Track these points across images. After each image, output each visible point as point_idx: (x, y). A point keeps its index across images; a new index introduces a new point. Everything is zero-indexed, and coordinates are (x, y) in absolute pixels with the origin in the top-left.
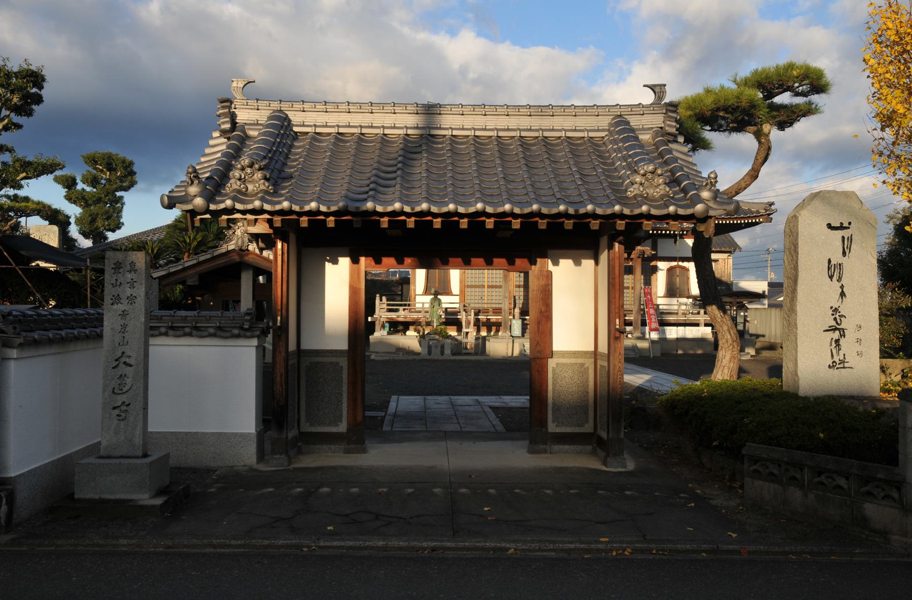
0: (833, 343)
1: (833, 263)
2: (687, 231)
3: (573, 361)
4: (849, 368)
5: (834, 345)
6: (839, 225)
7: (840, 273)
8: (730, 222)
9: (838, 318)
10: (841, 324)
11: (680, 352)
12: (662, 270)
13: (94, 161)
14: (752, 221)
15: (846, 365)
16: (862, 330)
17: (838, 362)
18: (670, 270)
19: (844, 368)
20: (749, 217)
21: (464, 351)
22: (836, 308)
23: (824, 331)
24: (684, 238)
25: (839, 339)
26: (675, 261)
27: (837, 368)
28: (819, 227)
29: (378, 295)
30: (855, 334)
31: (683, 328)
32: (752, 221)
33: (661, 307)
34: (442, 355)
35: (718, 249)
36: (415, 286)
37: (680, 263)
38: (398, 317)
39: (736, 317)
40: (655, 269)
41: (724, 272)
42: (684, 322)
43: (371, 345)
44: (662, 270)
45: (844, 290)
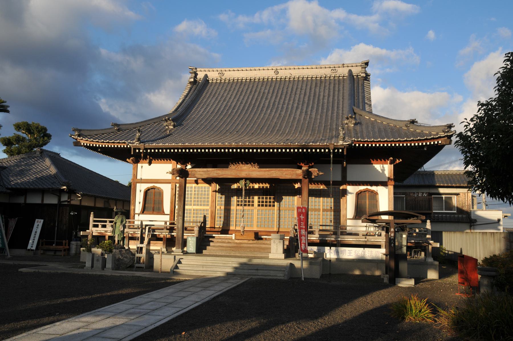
3: (223, 278)
11: (357, 272)
12: (351, 193)
13: (19, 127)
18: (359, 194)
21: (137, 265)
24: (372, 164)
26: (364, 185)
29: (92, 213)
31: (362, 249)
33: (348, 228)
35: (458, 185)
37: (369, 187)
38: (106, 231)
39: (394, 240)
40: (345, 193)
41: (465, 203)
42: (364, 243)
44: (351, 193)
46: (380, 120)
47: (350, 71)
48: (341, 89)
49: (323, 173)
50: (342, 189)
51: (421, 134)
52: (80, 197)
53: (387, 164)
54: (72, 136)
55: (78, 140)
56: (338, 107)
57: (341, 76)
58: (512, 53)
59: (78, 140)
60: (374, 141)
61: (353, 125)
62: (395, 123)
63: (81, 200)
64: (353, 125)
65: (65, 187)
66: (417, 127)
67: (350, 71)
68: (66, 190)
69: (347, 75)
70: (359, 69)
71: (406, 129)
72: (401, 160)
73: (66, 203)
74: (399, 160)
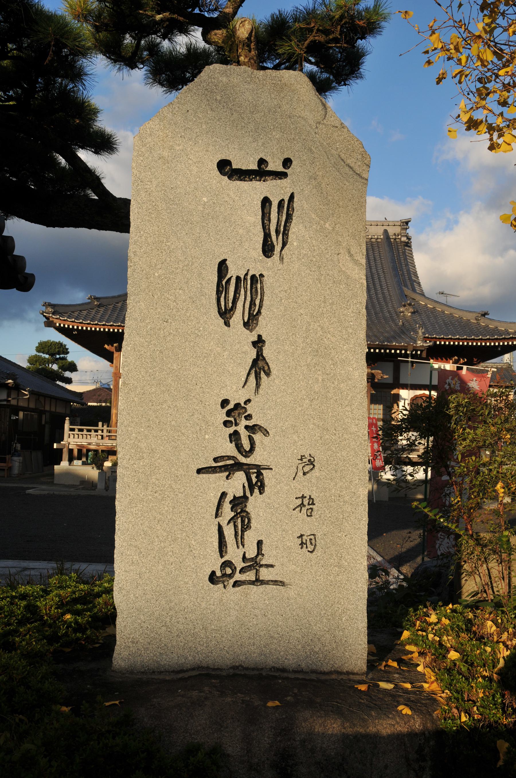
0: (227, 506)
1: (233, 272)
2: (422, 351)
4: (275, 582)
5: (227, 512)
6: (254, 167)
7: (252, 303)
8: (481, 343)
9: (244, 434)
10: (252, 449)
14: (508, 343)
15: (265, 574)
16: (316, 472)
17: (240, 565)
19: (258, 581)
20: (505, 339)
22: (237, 406)
23: (199, 471)
25: (245, 498)
26: (420, 389)
27: (236, 584)
28: (195, 169)
30: (295, 483)
32: (508, 343)
34: (107, 490)
36: (117, 409)
43: (55, 476)
45: (266, 352)
46: (440, 308)
47: (386, 231)
48: (378, 258)
49: (387, 376)
50: (394, 394)
51: (496, 331)
52: (27, 395)
53: (449, 363)
54: (44, 314)
55: (51, 319)
56: (381, 286)
57: (373, 237)
58: (514, 119)
59: (51, 319)
60: (443, 338)
61: (409, 314)
62: (461, 314)
63: (29, 398)
64: (409, 314)
65: (10, 381)
66: (491, 322)
67: (386, 231)
68: (13, 385)
69: (382, 237)
70: (398, 230)
71: (475, 323)
72: (466, 360)
73: (5, 403)
74: (464, 360)
